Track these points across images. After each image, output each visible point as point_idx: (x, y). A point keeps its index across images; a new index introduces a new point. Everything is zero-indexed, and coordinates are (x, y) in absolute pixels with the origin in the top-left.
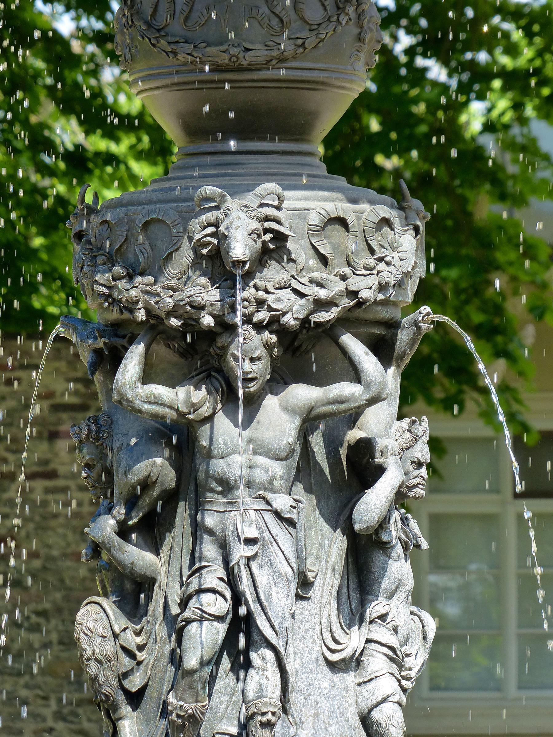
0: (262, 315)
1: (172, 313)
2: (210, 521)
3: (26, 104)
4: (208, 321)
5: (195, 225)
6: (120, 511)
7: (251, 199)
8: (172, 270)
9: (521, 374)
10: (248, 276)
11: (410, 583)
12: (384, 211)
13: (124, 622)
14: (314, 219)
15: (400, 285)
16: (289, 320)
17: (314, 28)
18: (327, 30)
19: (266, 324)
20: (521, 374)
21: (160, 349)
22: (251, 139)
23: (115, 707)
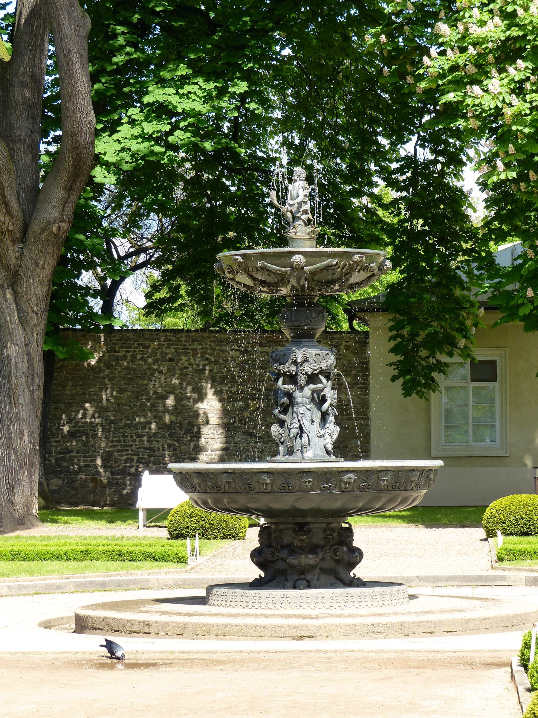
0: (304, 372)
1: (288, 372)
2: (295, 410)
3: (361, 126)
4: (294, 373)
5: (291, 355)
6: (279, 408)
7: (302, 351)
8: (287, 364)
9: (472, 343)
10: (301, 365)
11: (334, 421)
12: (327, 352)
13: (280, 428)
14: (314, 354)
15: (331, 365)
16: (309, 373)
17: (314, 318)
18: (316, 319)
19: (401, 314)
20: (472, 343)
21: (286, 378)
22: (183, 461)
23: (278, 445)
